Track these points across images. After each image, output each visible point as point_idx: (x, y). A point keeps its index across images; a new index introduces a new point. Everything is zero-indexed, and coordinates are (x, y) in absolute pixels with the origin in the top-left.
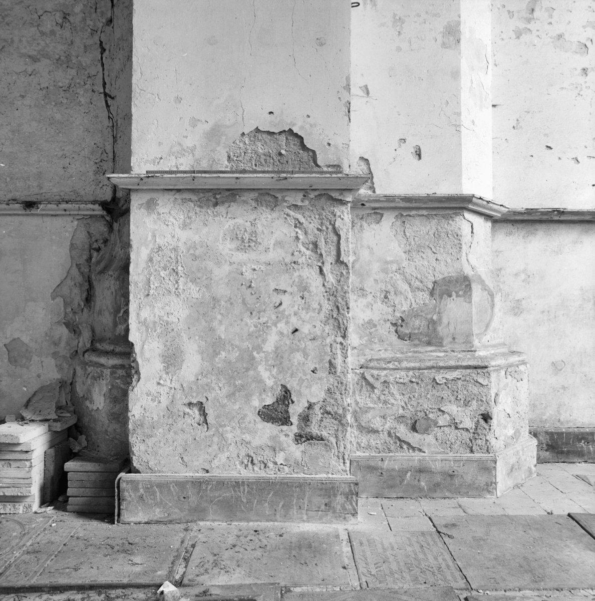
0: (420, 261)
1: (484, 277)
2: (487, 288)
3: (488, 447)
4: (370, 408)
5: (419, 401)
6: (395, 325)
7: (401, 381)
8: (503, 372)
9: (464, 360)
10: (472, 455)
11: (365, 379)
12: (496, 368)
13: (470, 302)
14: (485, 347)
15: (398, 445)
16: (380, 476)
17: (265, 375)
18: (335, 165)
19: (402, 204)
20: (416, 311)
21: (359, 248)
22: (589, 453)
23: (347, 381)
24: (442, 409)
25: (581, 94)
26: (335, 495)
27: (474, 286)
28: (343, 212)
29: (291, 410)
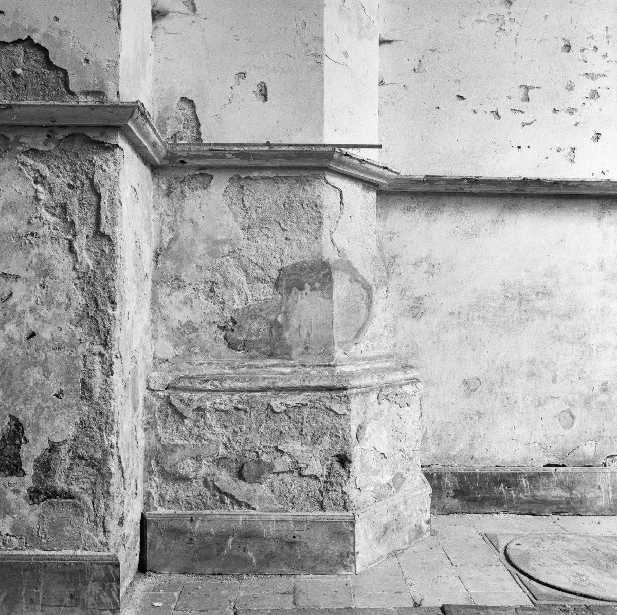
0: (263, 240)
1: (357, 263)
2: (360, 279)
3: (345, 502)
4: (177, 446)
5: (248, 436)
6: (223, 328)
7: (222, 407)
8: (373, 396)
9: (312, 379)
10: (322, 513)
11: (171, 404)
12: (363, 390)
13: (331, 298)
14: (355, 360)
15: (218, 498)
16: (189, 543)
18: (96, 92)
19: (237, 162)
20: (254, 309)
21: (179, 223)
22: (511, 500)
23: (109, 411)
24: (280, 447)
25: (503, 28)
26: (85, 583)
27: (336, 276)
28: (106, 161)
29: (23, 454)
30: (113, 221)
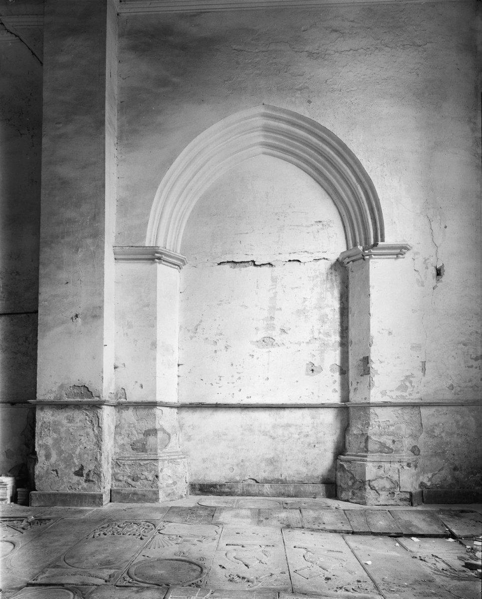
8: (166, 462)
17: (76, 461)
30: (102, 424)
